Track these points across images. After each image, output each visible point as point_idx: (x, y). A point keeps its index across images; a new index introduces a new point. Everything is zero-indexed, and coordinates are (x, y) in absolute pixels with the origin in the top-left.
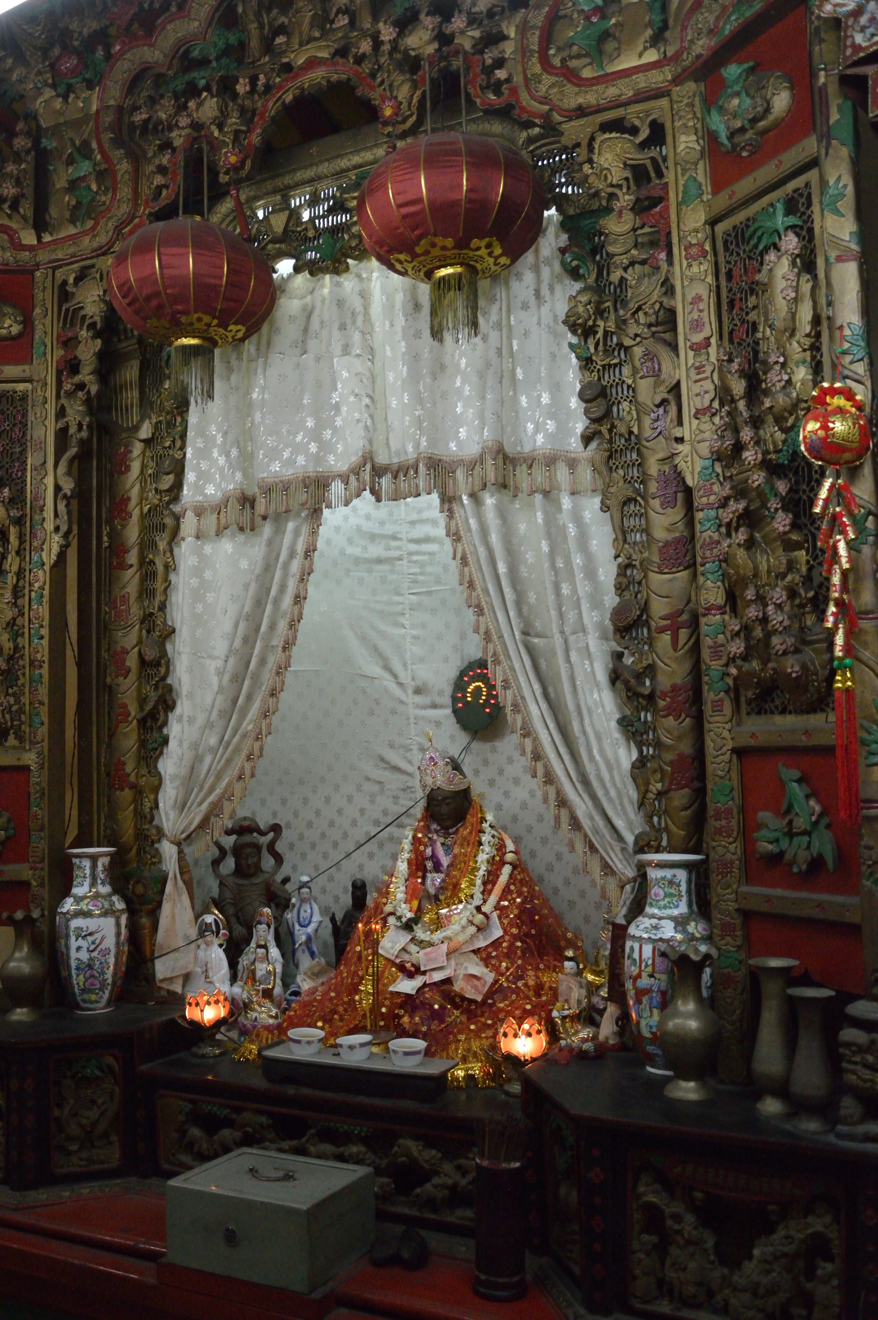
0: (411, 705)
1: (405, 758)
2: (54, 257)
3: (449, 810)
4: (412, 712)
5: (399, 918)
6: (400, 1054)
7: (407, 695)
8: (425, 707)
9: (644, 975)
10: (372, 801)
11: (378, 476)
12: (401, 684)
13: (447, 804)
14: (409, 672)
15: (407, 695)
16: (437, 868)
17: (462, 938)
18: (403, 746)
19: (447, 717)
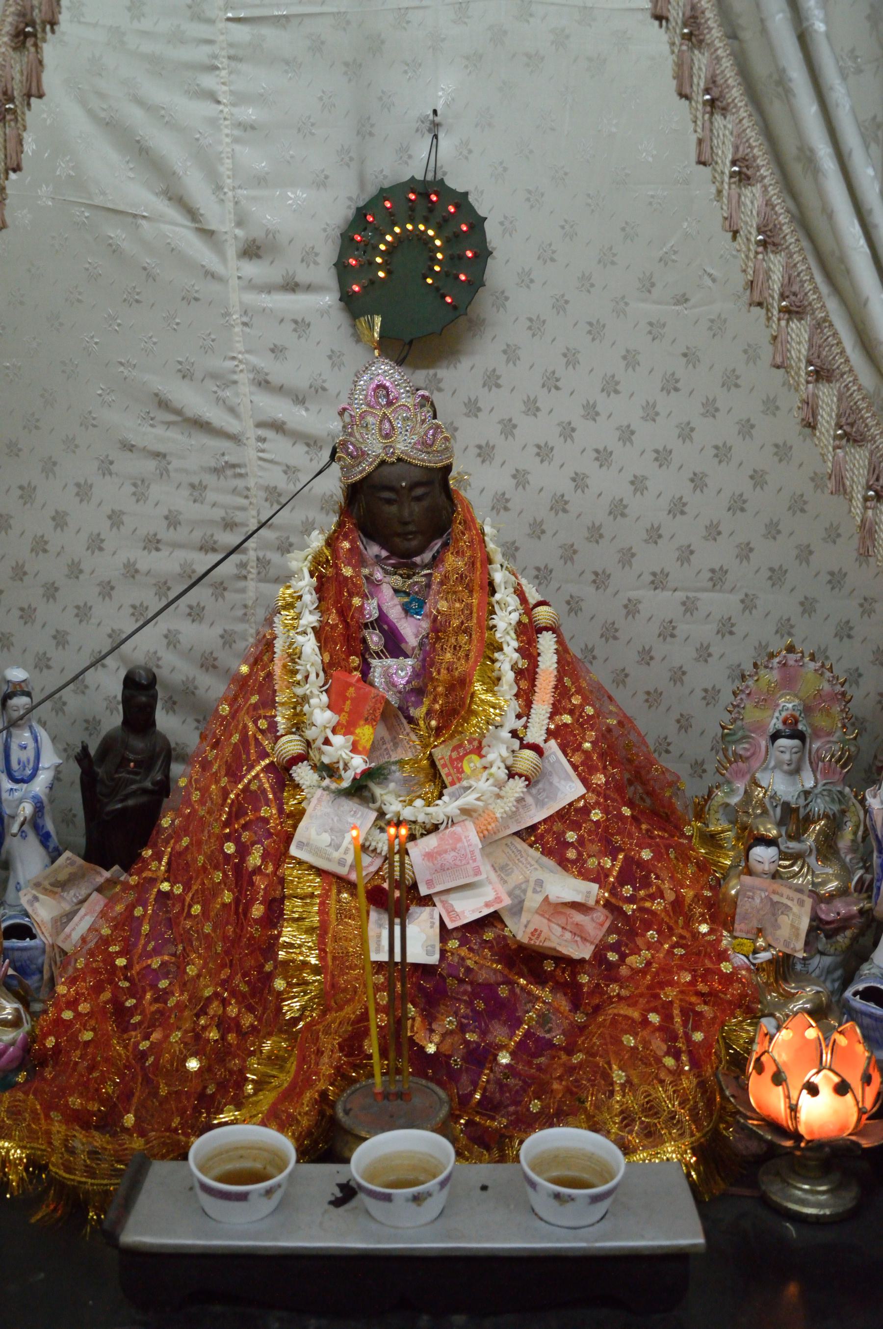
0: (234, 282)
1: (220, 401)
3: (401, 513)
4: (237, 297)
5: (330, 771)
7: (224, 259)
8: (269, 288)
10: (140, 497)
12: (207, 234)
13: (418, 499)
14: (230, 205)
15: (224, 259)
16: (394, 645)
17: (500, 809)
18: (214, 376)
19: (323, 313)
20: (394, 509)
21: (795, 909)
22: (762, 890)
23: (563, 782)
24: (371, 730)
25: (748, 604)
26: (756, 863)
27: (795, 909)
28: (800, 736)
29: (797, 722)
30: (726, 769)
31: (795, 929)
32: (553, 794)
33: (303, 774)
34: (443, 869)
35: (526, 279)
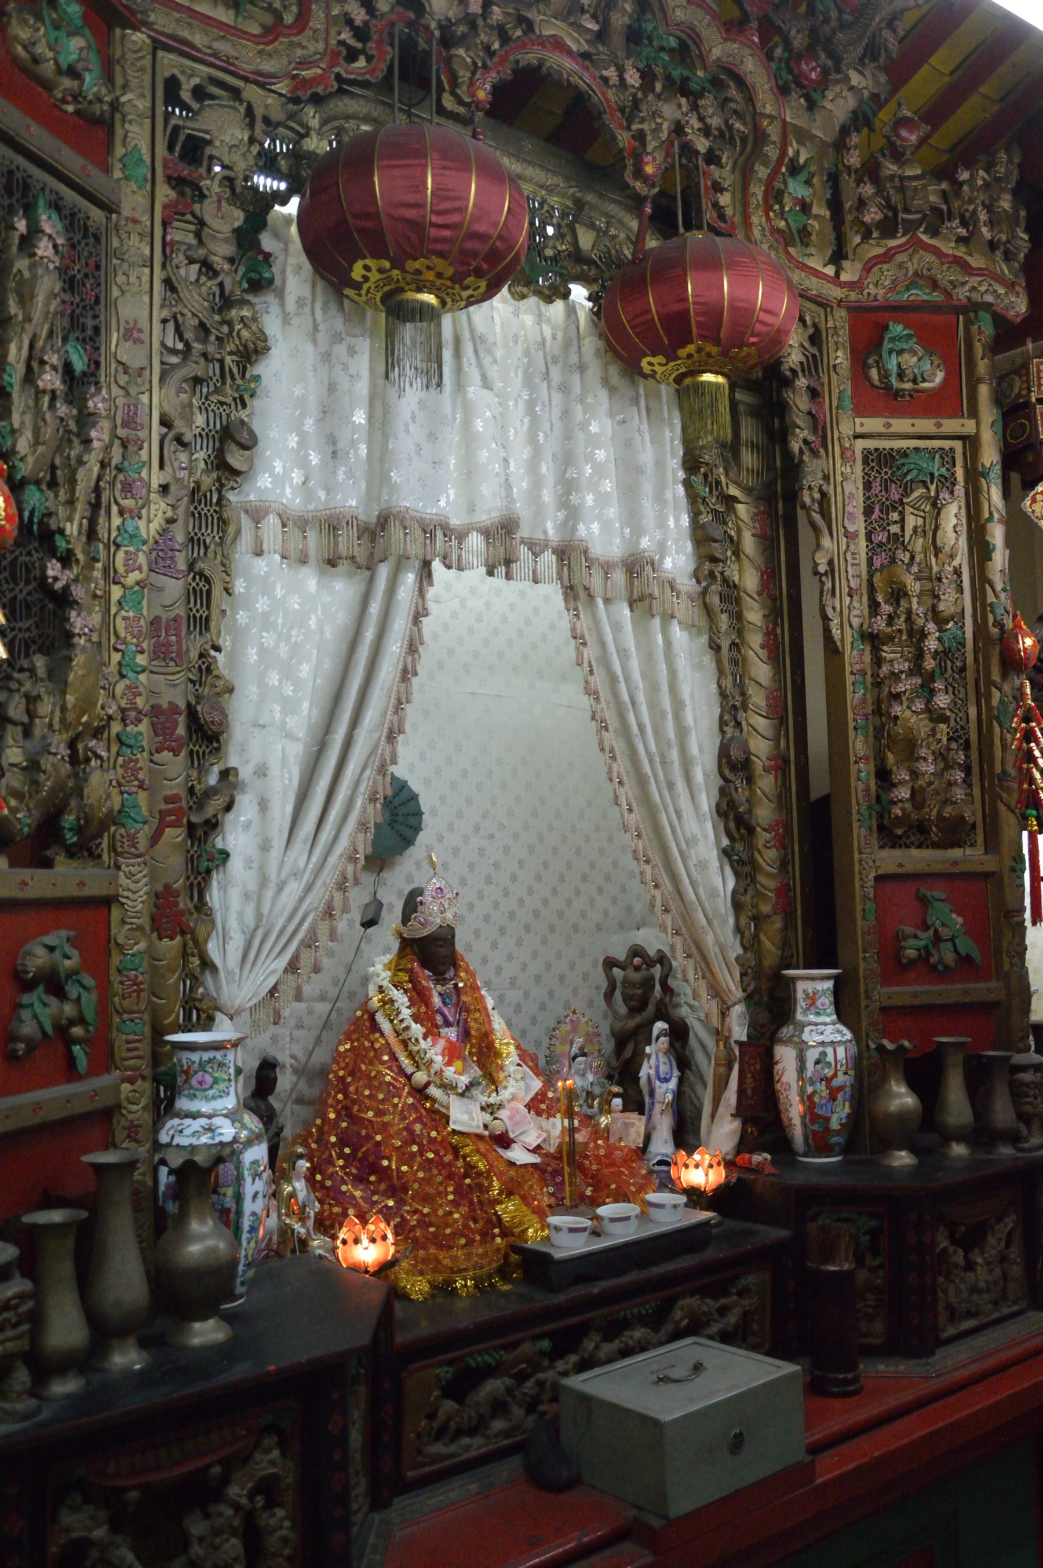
2: (185, 34)
3: (430, 955)
6: (565, 1231)
9: (840, 1074)
11: (504, 546)
21: (637, 1123)
24: (628, 481)
25: (526, 995)
27: (637, 1123)
28: (584, 1055)
31: (638, 1133)
33: (434, 1091)
35: (435, 636)
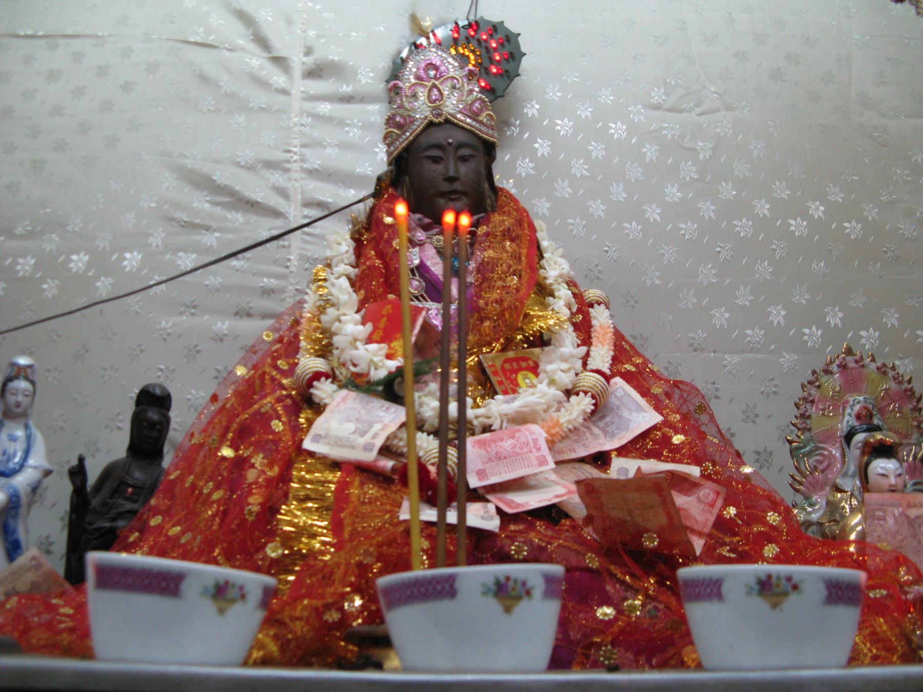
13: (464, 159)
20: (439, 168)
22: (895, 506)
23: (634, 414)
26: (880, 478)
29: (871, 416)
30: (800, 483)
32: (624, 425)
34: (499, 457)
